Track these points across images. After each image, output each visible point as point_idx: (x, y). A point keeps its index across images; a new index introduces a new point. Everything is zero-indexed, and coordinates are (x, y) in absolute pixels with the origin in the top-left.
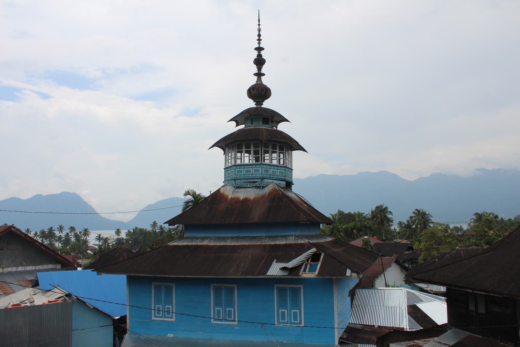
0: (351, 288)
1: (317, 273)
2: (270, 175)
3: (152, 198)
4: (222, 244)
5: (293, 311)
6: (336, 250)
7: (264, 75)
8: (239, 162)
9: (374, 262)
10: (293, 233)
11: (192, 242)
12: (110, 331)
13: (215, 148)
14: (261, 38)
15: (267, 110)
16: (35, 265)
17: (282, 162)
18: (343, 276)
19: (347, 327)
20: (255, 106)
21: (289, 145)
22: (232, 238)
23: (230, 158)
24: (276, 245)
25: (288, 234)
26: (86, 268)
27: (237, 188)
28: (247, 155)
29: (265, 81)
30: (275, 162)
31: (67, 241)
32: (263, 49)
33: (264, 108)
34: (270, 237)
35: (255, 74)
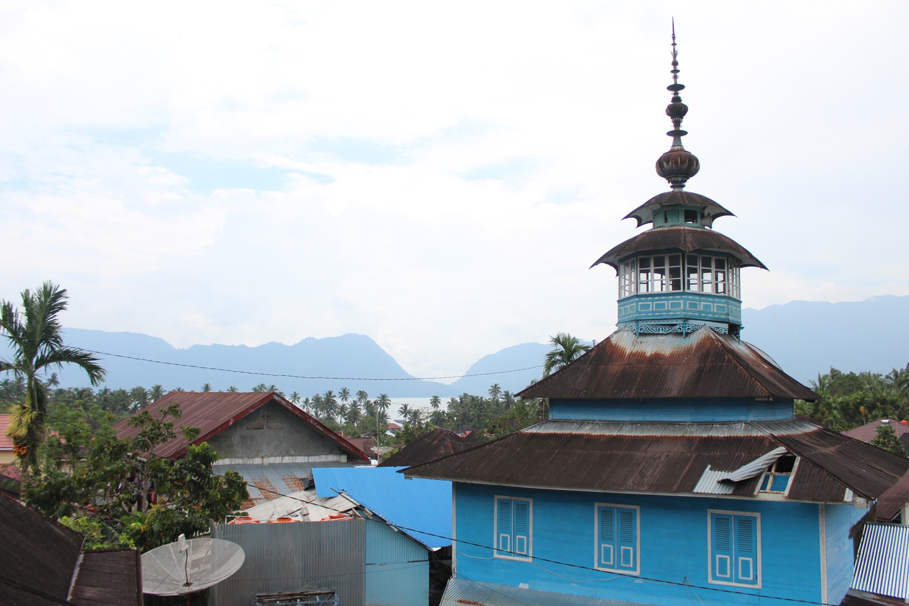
0: (855, 522)
1: (787, 492)
2: (700, 312)
3: (492, 343)
4: (615, 433)
5: (741, 558)
6: (824, 450)
7: (685, 133)
8: (643, 289)
9: (901, 475)
10: (743, 418)
11: (562, 428)
12: (424, 570)
13: (602, 265)
14: (678, 68)
15: (692, 197)
16: (309, 455)
17: (721, 289)
18: (837, 501)
19: (847, 596)
20: (671, 190)
21: (732, 257)
22: (632, 423)
23: (627, 282)
24: (710, 439)
25: (732, 419)
26: (386, 462)
27: (641, 334)
28: (657, 276)
29: (687, 143)
30: (708, 289)
31: (353, 415)
32: (682, 87)
33: (687, 193)
34: (700, 424)
35: (669, 134)
